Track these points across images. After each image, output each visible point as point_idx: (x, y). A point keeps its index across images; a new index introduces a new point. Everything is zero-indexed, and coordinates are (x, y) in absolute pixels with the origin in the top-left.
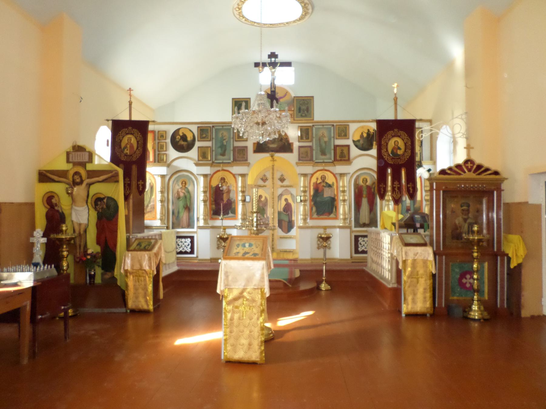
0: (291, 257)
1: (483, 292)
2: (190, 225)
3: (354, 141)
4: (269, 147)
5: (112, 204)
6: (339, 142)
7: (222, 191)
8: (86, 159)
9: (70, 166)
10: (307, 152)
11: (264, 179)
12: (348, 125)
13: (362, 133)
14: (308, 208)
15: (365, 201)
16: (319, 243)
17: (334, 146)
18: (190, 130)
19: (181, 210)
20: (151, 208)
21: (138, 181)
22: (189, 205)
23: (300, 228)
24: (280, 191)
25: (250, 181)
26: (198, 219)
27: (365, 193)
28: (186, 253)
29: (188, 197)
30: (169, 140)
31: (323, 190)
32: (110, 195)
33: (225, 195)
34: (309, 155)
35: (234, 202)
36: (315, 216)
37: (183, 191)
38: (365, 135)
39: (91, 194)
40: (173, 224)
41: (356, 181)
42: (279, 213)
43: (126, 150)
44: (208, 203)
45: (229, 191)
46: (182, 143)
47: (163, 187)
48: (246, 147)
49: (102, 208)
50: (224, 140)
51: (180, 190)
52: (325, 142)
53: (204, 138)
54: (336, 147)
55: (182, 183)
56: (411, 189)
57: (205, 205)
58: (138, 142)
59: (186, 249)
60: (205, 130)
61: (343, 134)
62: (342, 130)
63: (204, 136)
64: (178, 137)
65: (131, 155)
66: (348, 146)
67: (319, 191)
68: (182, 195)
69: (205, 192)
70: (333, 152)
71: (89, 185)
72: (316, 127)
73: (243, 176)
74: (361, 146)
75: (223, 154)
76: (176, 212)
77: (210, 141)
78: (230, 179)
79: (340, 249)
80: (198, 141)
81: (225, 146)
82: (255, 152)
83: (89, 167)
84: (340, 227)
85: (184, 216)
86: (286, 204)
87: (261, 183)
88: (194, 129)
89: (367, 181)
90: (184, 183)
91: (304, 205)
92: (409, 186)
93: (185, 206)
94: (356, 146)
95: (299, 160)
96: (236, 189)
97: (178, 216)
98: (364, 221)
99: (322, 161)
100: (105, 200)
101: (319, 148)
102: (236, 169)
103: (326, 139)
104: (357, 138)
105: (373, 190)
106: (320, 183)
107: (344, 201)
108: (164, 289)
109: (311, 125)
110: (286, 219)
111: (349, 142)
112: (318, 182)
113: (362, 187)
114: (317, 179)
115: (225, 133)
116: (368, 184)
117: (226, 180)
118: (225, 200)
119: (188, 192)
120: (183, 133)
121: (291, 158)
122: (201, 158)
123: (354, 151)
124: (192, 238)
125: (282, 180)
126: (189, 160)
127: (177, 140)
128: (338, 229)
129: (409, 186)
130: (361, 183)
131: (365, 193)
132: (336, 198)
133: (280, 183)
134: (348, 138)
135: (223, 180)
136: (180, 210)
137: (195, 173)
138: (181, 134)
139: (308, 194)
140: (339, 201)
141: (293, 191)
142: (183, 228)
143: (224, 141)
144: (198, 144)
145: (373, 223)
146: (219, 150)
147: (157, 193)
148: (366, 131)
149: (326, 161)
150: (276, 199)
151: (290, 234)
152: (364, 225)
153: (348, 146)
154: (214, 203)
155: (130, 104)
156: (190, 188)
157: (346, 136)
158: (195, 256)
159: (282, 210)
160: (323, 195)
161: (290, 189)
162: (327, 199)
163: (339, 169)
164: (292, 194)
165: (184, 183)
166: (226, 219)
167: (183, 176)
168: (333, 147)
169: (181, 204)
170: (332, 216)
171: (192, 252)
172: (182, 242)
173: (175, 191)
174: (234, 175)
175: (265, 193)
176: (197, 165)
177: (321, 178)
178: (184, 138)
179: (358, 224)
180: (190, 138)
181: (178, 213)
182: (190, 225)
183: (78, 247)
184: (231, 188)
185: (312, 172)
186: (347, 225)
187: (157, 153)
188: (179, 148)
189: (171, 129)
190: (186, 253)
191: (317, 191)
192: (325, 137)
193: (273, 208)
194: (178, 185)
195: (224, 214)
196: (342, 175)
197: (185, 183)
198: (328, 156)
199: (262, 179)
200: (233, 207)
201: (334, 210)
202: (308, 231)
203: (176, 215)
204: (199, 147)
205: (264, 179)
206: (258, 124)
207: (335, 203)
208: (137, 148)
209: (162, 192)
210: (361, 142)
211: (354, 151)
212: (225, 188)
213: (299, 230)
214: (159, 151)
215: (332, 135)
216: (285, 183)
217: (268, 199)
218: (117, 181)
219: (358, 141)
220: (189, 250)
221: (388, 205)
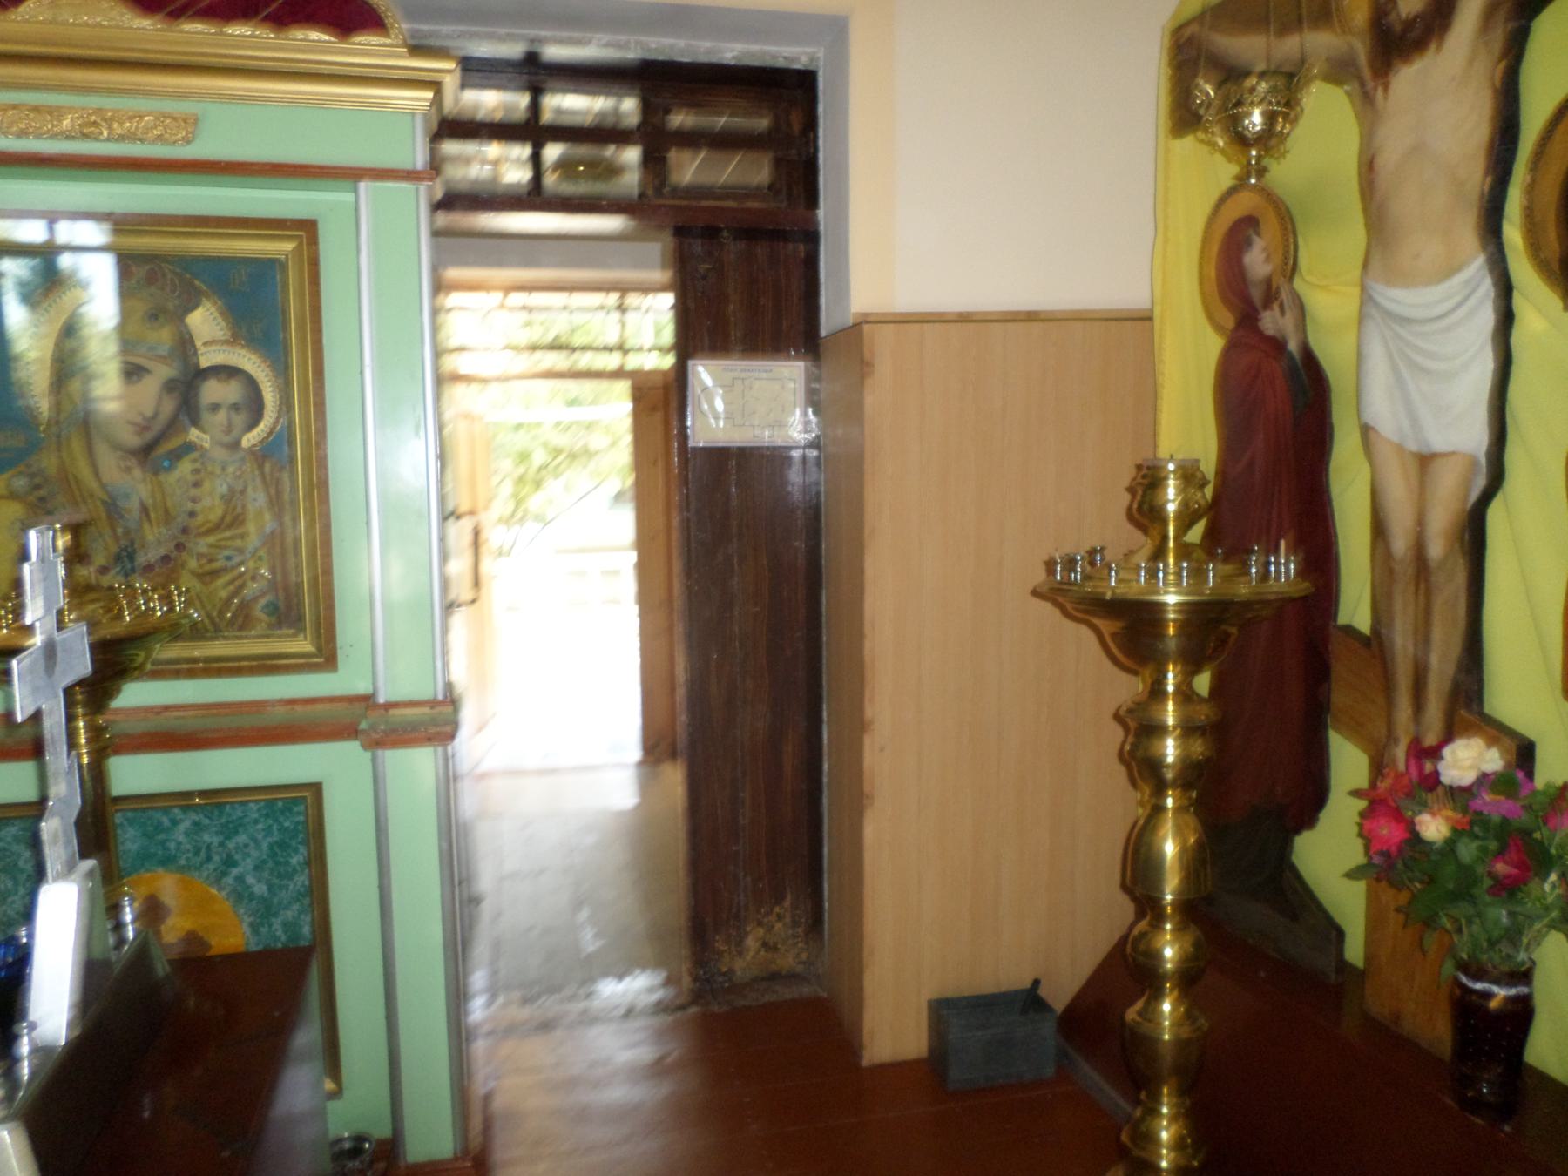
39: (1535, 114)
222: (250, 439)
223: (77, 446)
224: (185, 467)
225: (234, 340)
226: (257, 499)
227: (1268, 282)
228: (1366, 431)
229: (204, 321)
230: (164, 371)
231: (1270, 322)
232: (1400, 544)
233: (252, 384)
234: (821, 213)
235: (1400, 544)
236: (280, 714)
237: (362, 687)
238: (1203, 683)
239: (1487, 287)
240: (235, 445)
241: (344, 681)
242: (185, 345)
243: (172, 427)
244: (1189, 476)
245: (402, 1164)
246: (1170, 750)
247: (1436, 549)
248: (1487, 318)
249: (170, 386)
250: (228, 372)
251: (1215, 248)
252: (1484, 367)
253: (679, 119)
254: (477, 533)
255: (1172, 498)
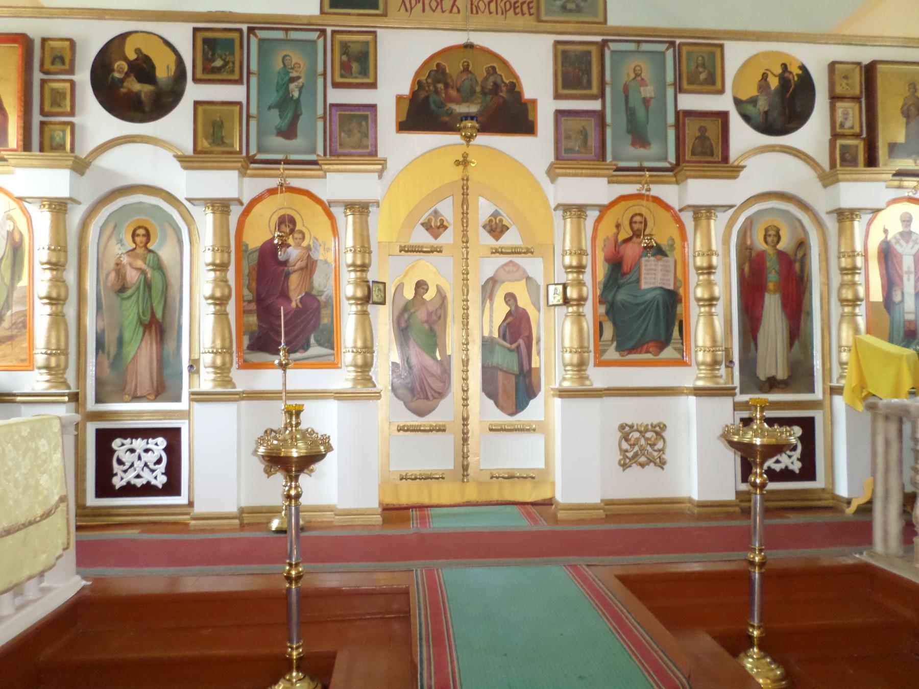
0: (528, 494)
2: (164, 387)
3: (738, 102)
4: (451, 113)
6: (690, 102)
7: (285, 263)
10: (584, 133)
11: (436, 227)
12: (721, 46)
13: (765, 77)
14: (588, 324)
15: (772, 305)
16: (625, 446)
17: (677, 113)
18: (167, 43)
19: (131, 332)
20: (13, 325)
22: (159, 315)
23: (564, 394)
24: (490, 266)
25: (381, 227)
26: (194, 367)
27: (772, 278)
28: (149, 490)
29: (157, 284)
30: (83, 76)
31: (637, 265)
33: (294, 279)
34: (593, 141)
35: (329, 303)
36: (612, 353)
37: (140, 263)
38: (774, 83)
40: (99, 383)
41: (744, 234)
42: (487, 345)
44: (231, 308)
45: (309, 266)
46: (135, 86)
47: (59, 246)
48: (373, 107)
50: (292, 80)
51: (125, 260)
52: (646, 102)
53: (218, 70)
54: (683, 116)
55: (134, 235)
57: (221, 315)
59: (147, 477)
60: (219, 48)
61: (703, 76)
62: (699, 61)
63: (218, 63)
64: (120, 67)
66: (723, 117)
67: (625, 268)
68: (132, 276)
69: (220, 267)
70: (671, 134)
72: (613, 46)
73: (360, 209)
74: (760, 119)
75: (289, 132)
76: (110, 340)
77: (239, 82)
78: (312, 223)
79: (698, 468)
80: (195, 80)
81: (298, 101)
82: (403, 127)
84: (699, 392)
85: (142, 354)
86: (509, 314)
87: (422, 237)
88: (182, 37)
89: (778, 238)
90: (143, 235)
91: (579, 316)
93: (147, 319)
94: (747, 118)
95: (557, 157)
96: (333, 257)
97: (119, 356)
98: (772, 373)
99: (635, 164)
101: (624, 118)
102: (339, 184)
103: (648, 91)
104: (750, 91)
105: (797, 266)
106: (626, 241)
107: (711, 301)
108: (285, 336)
109: (598, 39)
110: (510, 362)
111: (723, 103)
112: (623, 236)
113: (762, 255)
114: (618, 226)
115: (296, 57)
116: (781, 246)
117: (299, 227)
118: (296, 296)
119: (159, 267)
120: (138, 51)
121: (533, 151)
122: (204, 144)
123: (742, 136)
124: (172, 436)
125: (496, 228)
126: (160, 151)
127: (117, 75)
128: (693, 399)
130: (760, 244)
131: (772, 278)
132: (681, 291)
133: (487, 240)
134: (722, 91)
135: (287, 223)
136: (127, 335)
137: (181, 196)
138: (132, 56)
139: (587, 277)
140: (693, 304)
141: (533, 266)
142: (136, 398)
143: (292, 86)
144: (193, 92)
145: (799, 375)
146: (275, 119)
147: (38, 268)
148: (779, 70)
149: (647, 164)
150: (475, 296)
151: (523, 416)
152: (772, 384)
153: (723, 117)
154: (253, 306)
156: (166, 253)
157: (713, 83)
158: (182, 500)
159: (496, 335)
160: (638, 281)
161: (521, 261)
162: (649, 296)
163: (701, 190)
164: (528, 279)
165: (143, 235)
166: (299, 365)
167: (139, 207)
168: (671, 119)
169: (131, 311)
170: (669, 353)
171: (172, 487)
172: (132, 451)
173: (110, 264)
174: (327, 208)
175: (437, 272)
176: (186, 162)
177: (631, 223)
178: (143, 68)
179: (752, 380)
180: (164, 71)
181: (120, 342)
182: (164, 387)
184: (319, 255)
185: (606, 201)
186: (722, 382)
187: (37, 118)
188: (117, 102)
189: (93, 38)
190: (149, 490)
191: (618, 271)
192: (643, 83)
193: (466, 325)
194: (120, 242)
195: (290, 351)
196: (703, 213)
197: (148, 235)
198: (654, 149)
199: (427, 226)
200: (325, 321)
201: (676, 333)
202: (593, 405)
203: (113, 350)
204: (197, 103)
205: (436, 227)
207: (680, 309)
209: (56, 266)
210: (763, 105)
211: (742, 136)
212: (293, 253)
213: (558, 401)
214: (42, 113)
215: (670, 77)
216: (510, 239)
217: (450, 296)
219: (753, 101)
220: (160, 480)
221: (854, 315)
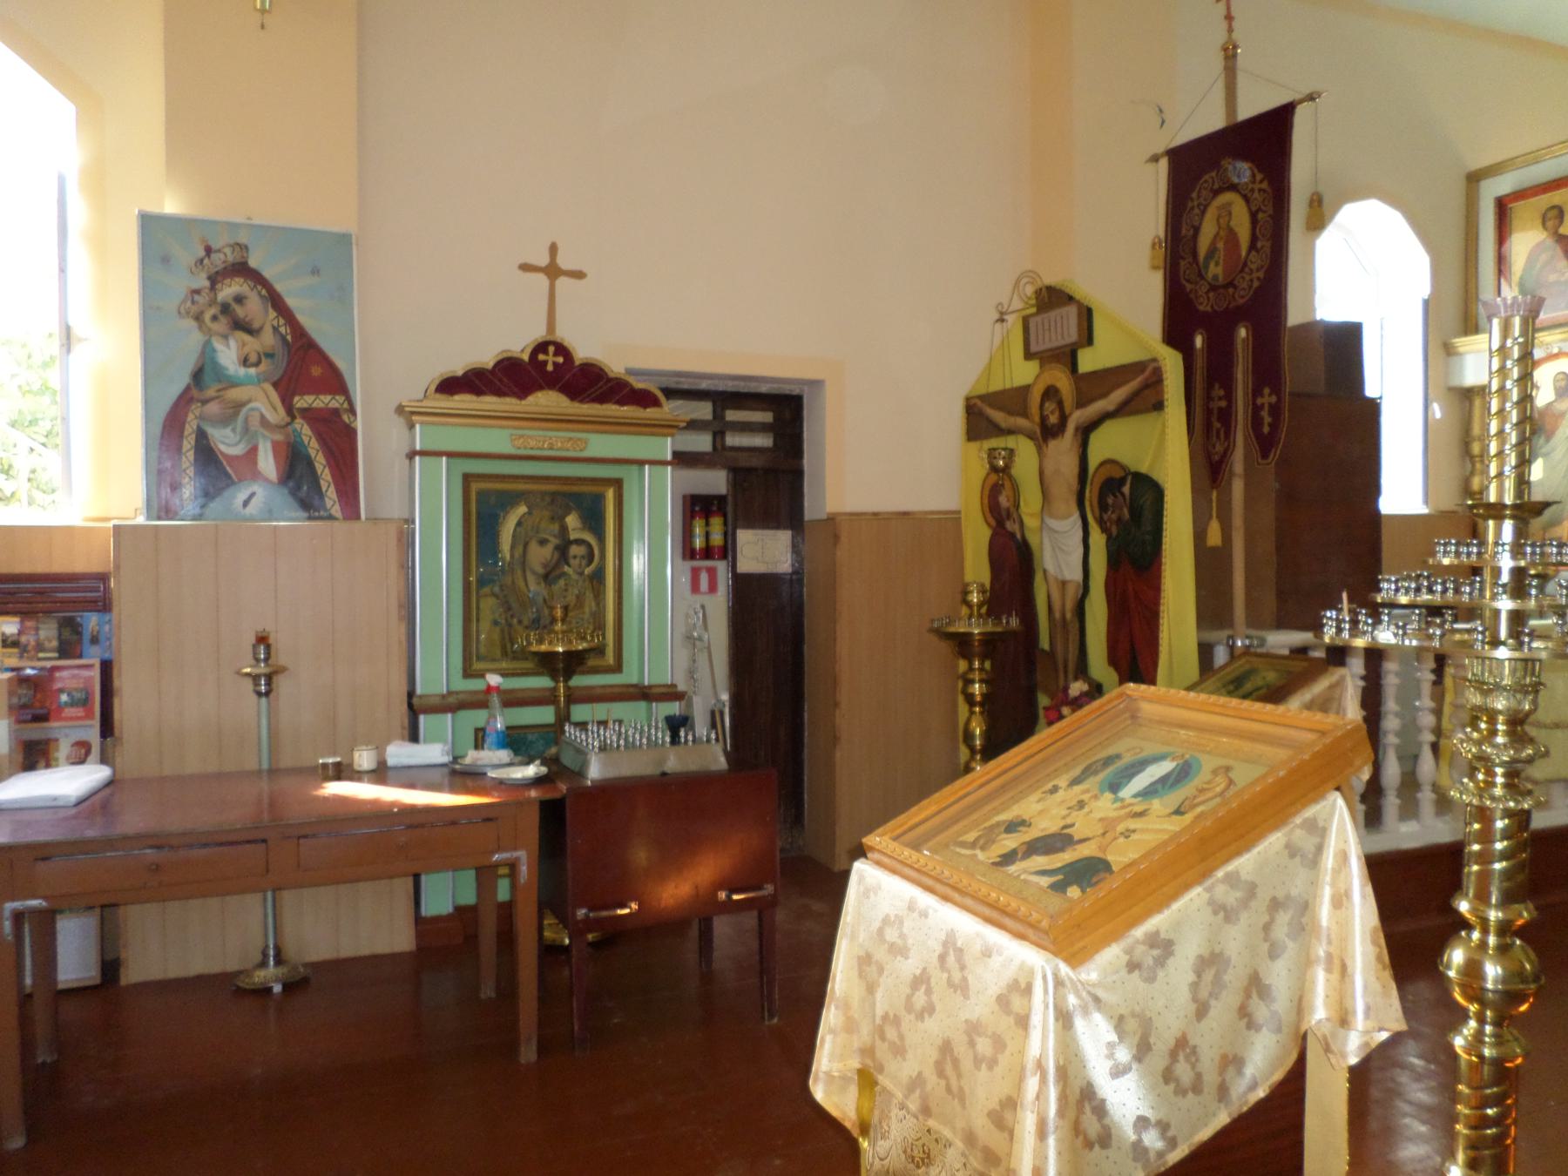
1: (1057, 1019)
5: (1147, 500)
8: (1072, 334)
9: (1033, 367)
21: (1257, 392)
32: (1144, 469)
39: (1093, 463)
43: (1212, 265)
49: (1119, 520)
56: (1266, 416)
58: (1254, 221)
65: (1231, 284)
71: (1086, 431)
83: (1088, 361)
92: (1259, 401)
100: (1126, 489)
129: (1223, 404)
155: (1230, 54)
183: (1061, 667)
206: (33, 471)
208: (1253, 246)
218: (1159, 406)
222: (587, 571)
223: (519, 572)
224: (562, 582)
225: (583, 529)
226: (589, 595)
227: (1008, 510)
228: (1045, 571)
229: (572, 520)
230: (554, 541)
231: (1009, 526)
232: (1057, 615)
233: (589, 546)
234: (805, 461)
235: (1057, 615)
236: (599, 691)
237: (634, 680)
238: (987, 665)
239: (1079, 523)
240: (581, 574)
241: (629, 676)
242: (564, 529)
243: (557, 565)
244: (982, 591)
245: (1294, 318)
246: (977, 688)
247: (1069, 616)
248: (1080, 534)
249: (557, 548)
250: (579, 542)
251: (987, 492)
252: (1081, 550)
253: (732, 415)
254: (107, 668)
255: (975, 598)
